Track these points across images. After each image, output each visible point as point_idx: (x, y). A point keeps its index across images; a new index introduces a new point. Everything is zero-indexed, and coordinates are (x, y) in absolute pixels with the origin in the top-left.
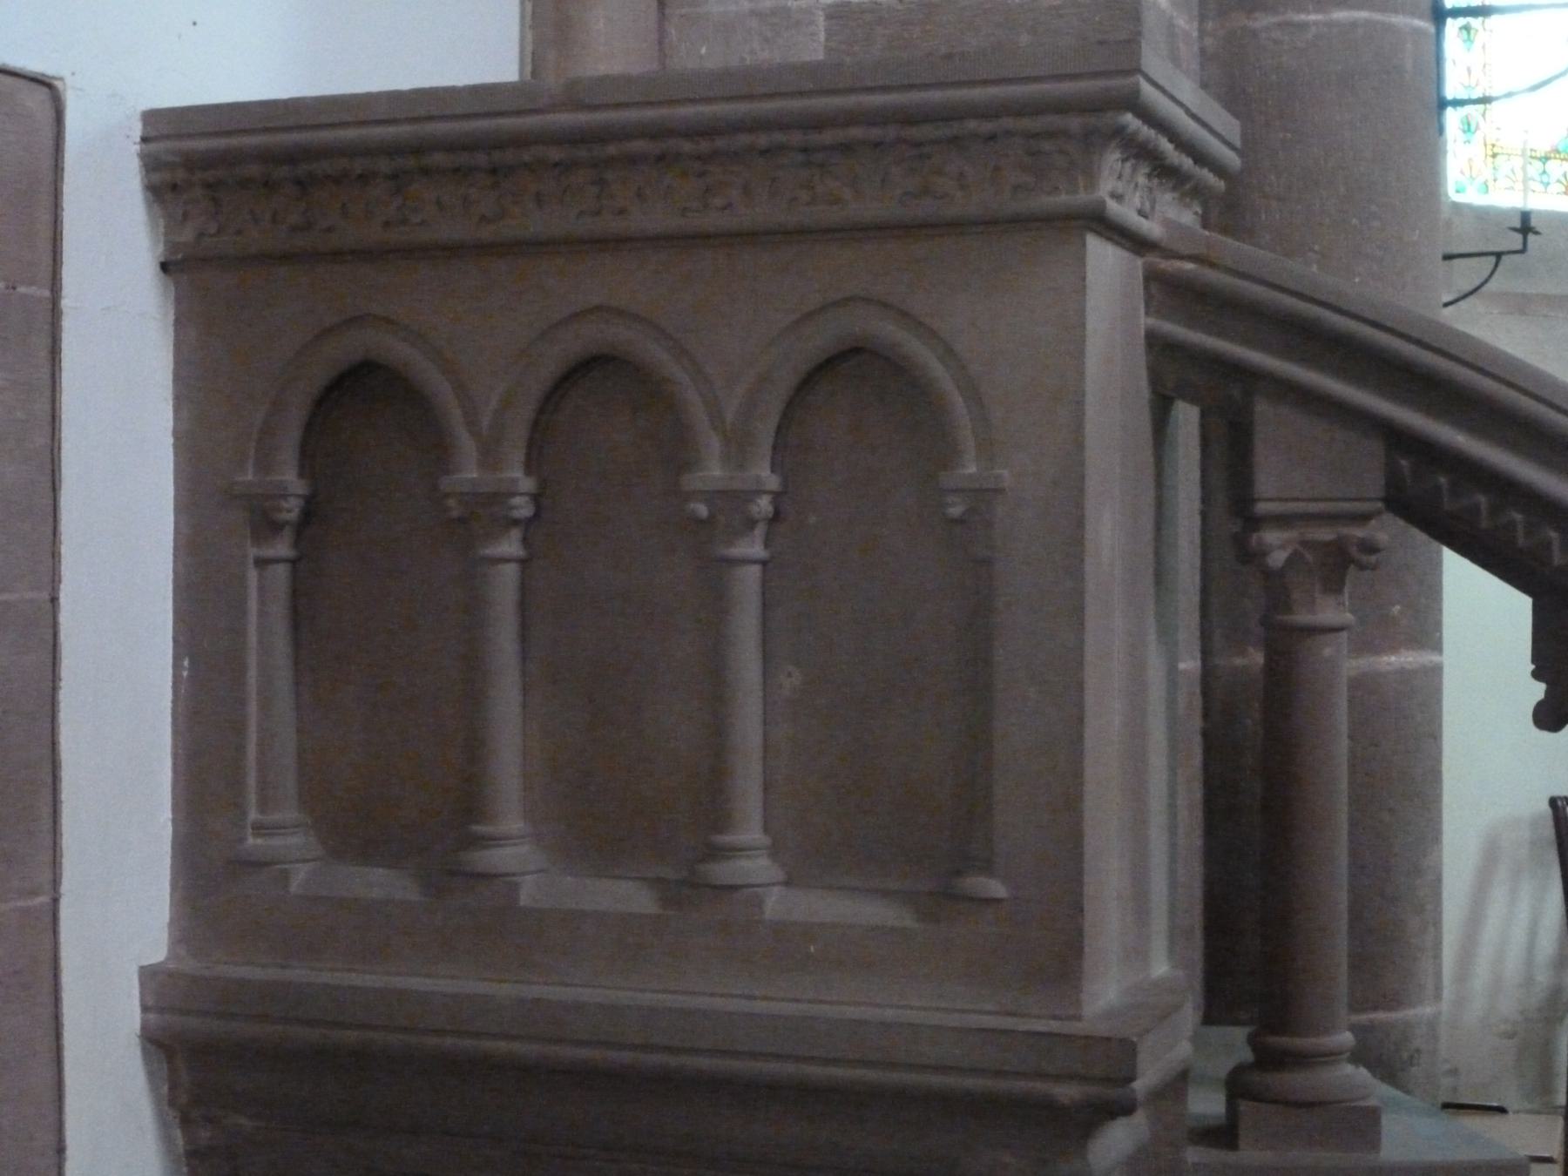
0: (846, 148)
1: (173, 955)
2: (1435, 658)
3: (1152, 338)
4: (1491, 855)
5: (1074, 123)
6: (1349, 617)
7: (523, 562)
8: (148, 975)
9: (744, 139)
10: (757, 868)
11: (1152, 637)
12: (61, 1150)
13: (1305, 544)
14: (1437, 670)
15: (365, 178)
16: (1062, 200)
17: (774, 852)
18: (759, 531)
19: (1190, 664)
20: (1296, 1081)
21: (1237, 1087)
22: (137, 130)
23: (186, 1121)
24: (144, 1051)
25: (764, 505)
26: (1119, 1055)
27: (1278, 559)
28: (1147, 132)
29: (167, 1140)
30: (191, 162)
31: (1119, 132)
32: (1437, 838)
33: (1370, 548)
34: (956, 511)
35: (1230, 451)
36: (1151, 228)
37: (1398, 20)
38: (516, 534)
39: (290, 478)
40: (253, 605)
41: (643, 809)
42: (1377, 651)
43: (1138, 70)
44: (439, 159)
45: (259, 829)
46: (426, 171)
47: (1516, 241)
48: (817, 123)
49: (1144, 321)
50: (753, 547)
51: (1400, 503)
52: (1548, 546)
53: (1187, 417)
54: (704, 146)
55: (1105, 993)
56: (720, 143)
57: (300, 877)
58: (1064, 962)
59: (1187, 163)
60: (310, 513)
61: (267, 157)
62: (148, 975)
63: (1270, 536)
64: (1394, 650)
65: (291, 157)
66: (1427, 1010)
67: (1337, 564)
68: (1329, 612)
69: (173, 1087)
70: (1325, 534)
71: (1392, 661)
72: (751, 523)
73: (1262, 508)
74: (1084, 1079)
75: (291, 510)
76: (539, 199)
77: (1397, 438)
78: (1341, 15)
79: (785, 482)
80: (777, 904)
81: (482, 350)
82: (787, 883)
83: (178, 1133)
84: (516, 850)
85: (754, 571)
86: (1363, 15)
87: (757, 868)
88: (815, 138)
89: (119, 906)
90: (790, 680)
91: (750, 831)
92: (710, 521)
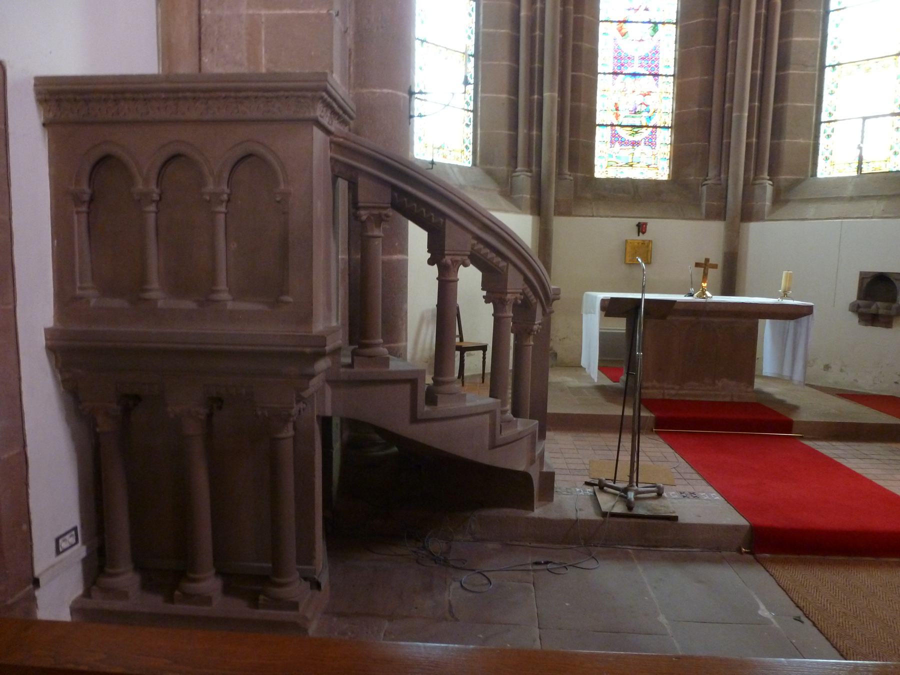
0: (247, 98)
1: (55, 324)
2: (405, 257)
3: (331, 158)
4: (422, 319)
5: (309, 94)
6: (381, 234)
7: (157, 213)
8: (47, 331)
9: (219, 94)
10: (225, 296)
11: (332, 239)
12: (20, 379)
13: (373, 215)
14: (407, 260)
15: (105, 100)
16: (307, 115)
17: (230, 291)
18: (224, 205)
19: (343, 256)
20: (368, 351)
21: (354, 354)
22: (33, 82)
23: (61, 372)
24: (47, 353)
25: (225, 197)
26: (321, 340)
27: (364, 218)
28: (329, 100)
29: (55, 376)
30: (51, 93)
31: (322, 98)
32: (406, 302)
33: (387, 216)
34: (278, 199)
35: (353, 187)
36: (332, 128)
37: (400, 93)
38: (154, 204)
39: (85, 187)
40: (76, 225)
41: (191, 282)
42: (391, 254)
43: (327, 80)
44: (128, 95)
45: (81, 288)
46: (125, 99)
47: (430, 166)
48: (238, 90)
49: (329, 154)
50: (222, 208)
51: (397, 207)
52: (431, 217)
53: (342, 184)
54: (207, 95)
55: (319, 327)
56: (212, 94)
57: (93, 302)
58: (307, 318)
59: (341, 112)
60: (92, 200)
61: (75, 92)
62: (47, 331)
63: (362, 212)
64: (396, 254)
65: (82, 93)
66: (404, 344)
67: (380, 220)
68: (377, 232)
69: (57, 362)
70: (376, 212)
71: (395, 257)
72: (222, 202)
73: (360, 204)
74: (311, 346)
75: (86, 197)
76: (159, 108)
77: (394, 188)
78: (385, 91)
79: (231, 190)
80: (230, 305)
81: (142, 151)
82: (233, 300)
83: (59, 376)
84: (156, 292)
85: (223, 216)
86: (390, 91)
87: (225, 296)
88: (238, 94)
89: (36, 309)
90: (234, 246)
91: (222, 285)
92: (209, 201)
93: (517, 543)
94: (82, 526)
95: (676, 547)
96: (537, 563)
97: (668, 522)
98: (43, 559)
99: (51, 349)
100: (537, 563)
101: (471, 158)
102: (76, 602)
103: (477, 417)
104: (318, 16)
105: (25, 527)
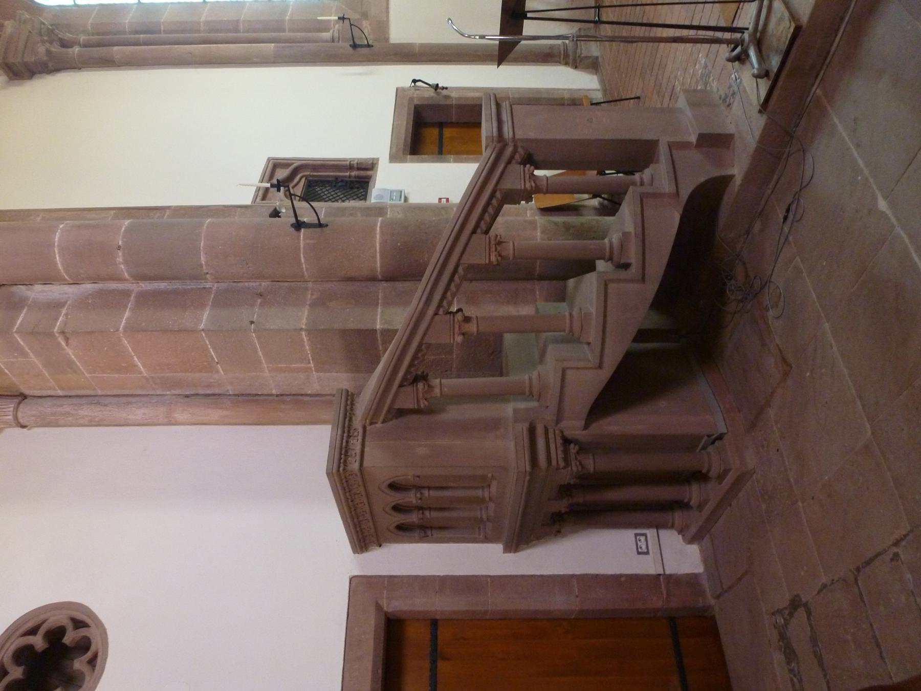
0: (347, 442)
86: (302, 256)
93: (763, 202)
94: (636, 528)
95: (838, 30)
96: (785, 218)
97: (798, 42)
98: (647, 566)
99: (516, 551)
100: (785, 218)
101: (439, 633)
102: (684, 540)
103: (608, 325)
104: (258, 338)
105: (623, 579)
